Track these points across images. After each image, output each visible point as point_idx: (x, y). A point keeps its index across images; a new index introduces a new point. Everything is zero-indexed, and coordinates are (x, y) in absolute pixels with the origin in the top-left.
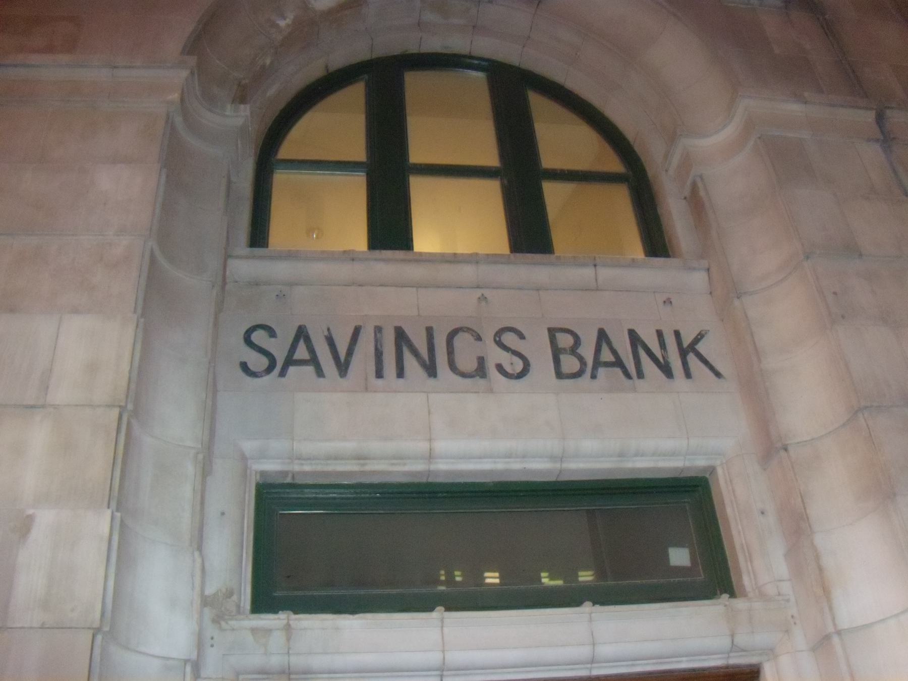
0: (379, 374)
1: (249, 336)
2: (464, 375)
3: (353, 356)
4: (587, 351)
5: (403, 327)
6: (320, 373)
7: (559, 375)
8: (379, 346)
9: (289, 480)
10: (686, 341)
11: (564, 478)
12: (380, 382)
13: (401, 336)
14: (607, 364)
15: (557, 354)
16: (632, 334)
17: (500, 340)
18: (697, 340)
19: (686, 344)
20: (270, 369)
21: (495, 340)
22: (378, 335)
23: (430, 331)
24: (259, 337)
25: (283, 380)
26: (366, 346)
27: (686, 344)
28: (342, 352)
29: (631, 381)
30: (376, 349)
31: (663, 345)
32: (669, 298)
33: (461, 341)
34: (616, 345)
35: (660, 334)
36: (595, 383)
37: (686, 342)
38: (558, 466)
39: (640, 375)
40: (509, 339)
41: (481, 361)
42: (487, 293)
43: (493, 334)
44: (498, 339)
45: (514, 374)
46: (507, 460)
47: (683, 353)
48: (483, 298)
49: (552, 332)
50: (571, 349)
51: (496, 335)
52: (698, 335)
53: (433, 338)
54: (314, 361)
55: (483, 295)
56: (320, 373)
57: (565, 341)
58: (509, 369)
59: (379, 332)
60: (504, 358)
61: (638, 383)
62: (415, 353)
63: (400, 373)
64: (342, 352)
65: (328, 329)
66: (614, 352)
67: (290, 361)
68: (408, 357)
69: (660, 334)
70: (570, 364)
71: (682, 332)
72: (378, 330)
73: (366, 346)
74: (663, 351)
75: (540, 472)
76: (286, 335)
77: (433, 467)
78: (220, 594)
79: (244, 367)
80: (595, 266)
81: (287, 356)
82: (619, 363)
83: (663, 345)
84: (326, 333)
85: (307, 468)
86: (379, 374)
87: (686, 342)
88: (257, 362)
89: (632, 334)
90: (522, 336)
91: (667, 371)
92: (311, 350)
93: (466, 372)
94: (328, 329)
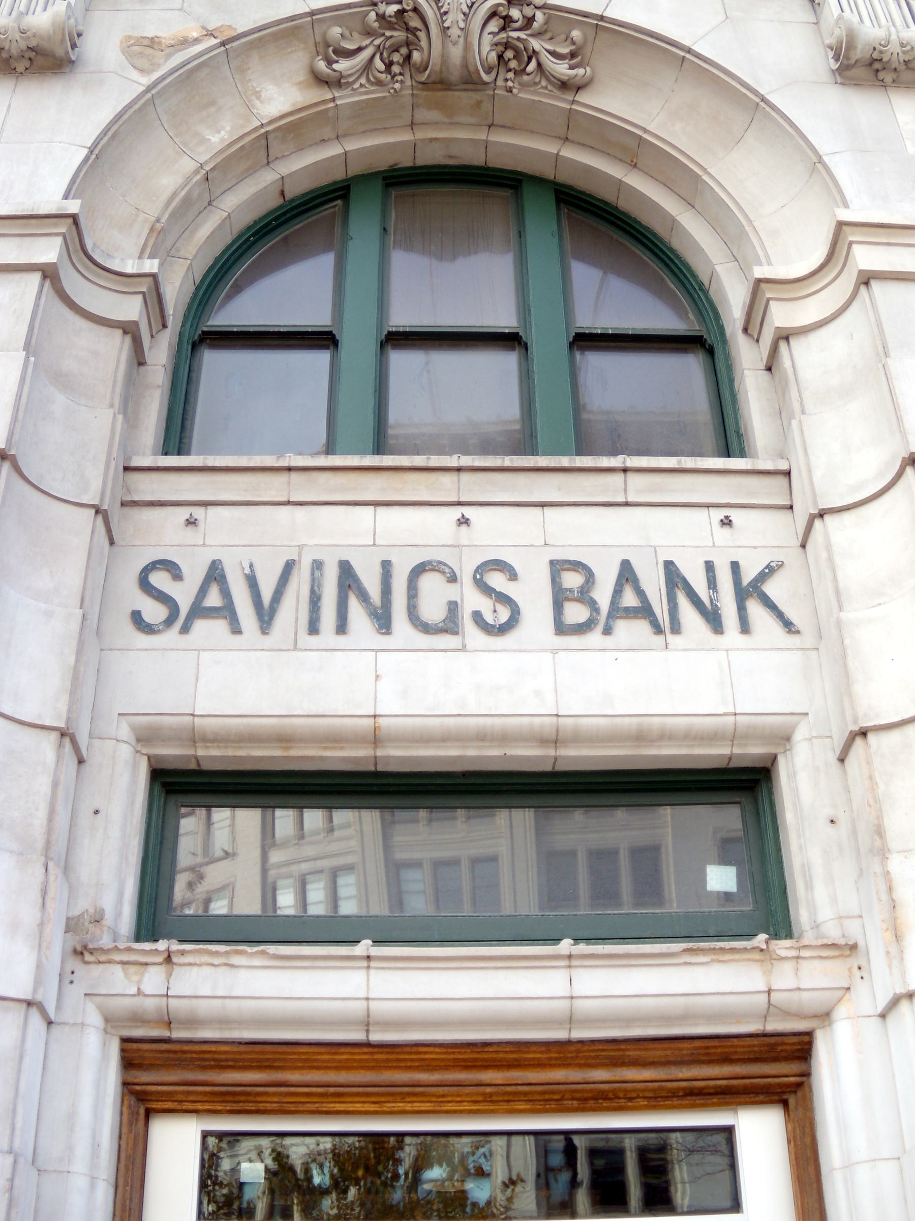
0: (314, 628)
1: (146, 577)
2: (426, 628)
3: (419, 8)
4: (603, 595)
5: (352, 563)
6: (236, 630)
7: (561, 628)
8: (316, 589)
9: (193, 766)
10: (749, 575)
11: (561, 767)
12: (314, 640)
13: (346, 572)
14: (630, 613)
15: (560, 598)
16: (669, 566)
17: (482, 578)
18: (768, 572)
19: (746, 580)
20: (169, 622)
21: (474, 577)
22: (317, 573)
23: (386, 566)
24: (159, 579)
25: (184, 637)
26: (300, 585)
27: (746, 580)
28: (267, 595)
29: (662, 637)
30: (312, 592)
31: (712, 583)
32: (727, 516)
33: (430, 583)
34: (645, 585)
35: (710, 567)
36: (608, 641)
37: (746, 578)
38: (552, 752)
39: (676, 628)
40: (497, 581)
41: (453, 608)
42: (468, 512)
43: (474, 568)
44: (478, 577)
45: (496, 625)
46: (481, 744)
47: (742, 594)
48: (464, 521)
49: (557, 567)
50: (579, 590)
51: (476, 571)
52: (767, 567)
53: (391, 576)
54: (228, 612)
55: (463, 515)
56: (236, 630)
57: (573, 580)
58: (489, 618)
59: (317, 569)
60: (484, 605)
61: (672, 639)
62: (364, 597)
63: (342, 628)
64: (267, 595)
65: (251, 566)
66: (640, 593)
67: (198, 611)
68: (355, 606)
69: (710, 567)
70: (576, 613)
71: (742, 563)
72: (318, 565)
73: (300, 585)
74: (711, 591)
75: (528, 759)
76: (195, 575)
77: (380, 753)
78: (85, 917)
79: (137, 618)
80: (83, 1024)
81: (194, 603)
82: (645, 611)
83: (712, 583)
84: (247, 571)
85: (215, 752)
86: (314, 628)
87: (746, 578)
88: (154, 612)
89: (669, 566)
90: (513, 576)
91: (713, 619)
92: (226, 594)
93: (430, 623)
94: (251, 566)
